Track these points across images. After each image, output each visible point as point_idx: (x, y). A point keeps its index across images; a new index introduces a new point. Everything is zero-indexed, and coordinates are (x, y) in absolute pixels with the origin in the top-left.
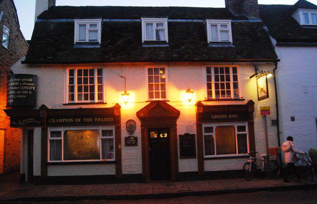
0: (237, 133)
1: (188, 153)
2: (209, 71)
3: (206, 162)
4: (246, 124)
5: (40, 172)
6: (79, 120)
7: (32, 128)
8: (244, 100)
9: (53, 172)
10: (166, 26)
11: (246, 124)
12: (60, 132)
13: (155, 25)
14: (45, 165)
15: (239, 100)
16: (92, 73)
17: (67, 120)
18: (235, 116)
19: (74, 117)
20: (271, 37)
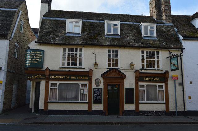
0: (80, 88)
1: (130, 101)
3: (140, 105)
6: (68, 77)
7: (39, 81)
9: (51, 107)
10: (155, 28)
11: (163, 84)
12: (56, 84)
14: (46, 103)
17: (61, 77)
19: (65, 75)
20: (179, 35)
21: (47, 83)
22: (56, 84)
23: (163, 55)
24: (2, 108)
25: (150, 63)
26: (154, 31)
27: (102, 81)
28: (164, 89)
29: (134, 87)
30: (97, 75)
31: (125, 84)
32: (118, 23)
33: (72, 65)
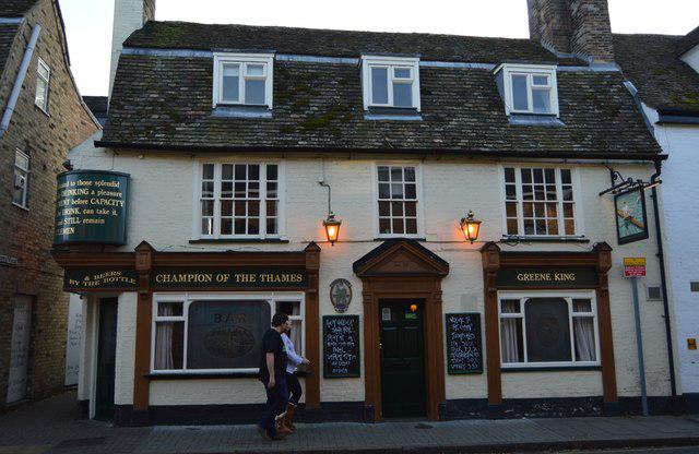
0: (572, 314)
2: (208, 172)
4: (592, 295)
5: (132, 397)
6: (225, 278)
7: (113, 295)
8: (587, 241)
9: (161, 395)
11: (592, 295)
14: (144, 379)
15: (278, 241)
16: (255, 173)
17: (197, 278)
18: (568, 277)
19: (214, 270)
21: (144, 301)
22: (515, 304)
23: (588, 185)
25: (540, 213)
26: (548, 91)
27: (357, 288)
28: (594, 313)
29: (479, 308)
30: (338, 265)
31: (444, 298)
32: (414, 65)
33: (240, 230)
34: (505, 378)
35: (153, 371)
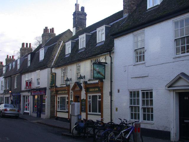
3: (88, 116)
13: (101, 30)
24: (50, 115)
29: (85, 99)
34: (88, 116)
35: (57, 110)
